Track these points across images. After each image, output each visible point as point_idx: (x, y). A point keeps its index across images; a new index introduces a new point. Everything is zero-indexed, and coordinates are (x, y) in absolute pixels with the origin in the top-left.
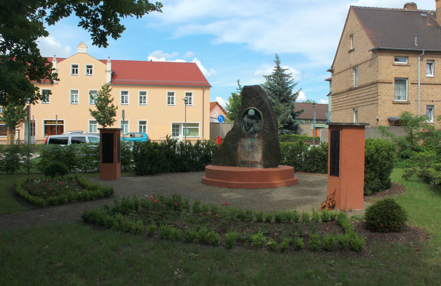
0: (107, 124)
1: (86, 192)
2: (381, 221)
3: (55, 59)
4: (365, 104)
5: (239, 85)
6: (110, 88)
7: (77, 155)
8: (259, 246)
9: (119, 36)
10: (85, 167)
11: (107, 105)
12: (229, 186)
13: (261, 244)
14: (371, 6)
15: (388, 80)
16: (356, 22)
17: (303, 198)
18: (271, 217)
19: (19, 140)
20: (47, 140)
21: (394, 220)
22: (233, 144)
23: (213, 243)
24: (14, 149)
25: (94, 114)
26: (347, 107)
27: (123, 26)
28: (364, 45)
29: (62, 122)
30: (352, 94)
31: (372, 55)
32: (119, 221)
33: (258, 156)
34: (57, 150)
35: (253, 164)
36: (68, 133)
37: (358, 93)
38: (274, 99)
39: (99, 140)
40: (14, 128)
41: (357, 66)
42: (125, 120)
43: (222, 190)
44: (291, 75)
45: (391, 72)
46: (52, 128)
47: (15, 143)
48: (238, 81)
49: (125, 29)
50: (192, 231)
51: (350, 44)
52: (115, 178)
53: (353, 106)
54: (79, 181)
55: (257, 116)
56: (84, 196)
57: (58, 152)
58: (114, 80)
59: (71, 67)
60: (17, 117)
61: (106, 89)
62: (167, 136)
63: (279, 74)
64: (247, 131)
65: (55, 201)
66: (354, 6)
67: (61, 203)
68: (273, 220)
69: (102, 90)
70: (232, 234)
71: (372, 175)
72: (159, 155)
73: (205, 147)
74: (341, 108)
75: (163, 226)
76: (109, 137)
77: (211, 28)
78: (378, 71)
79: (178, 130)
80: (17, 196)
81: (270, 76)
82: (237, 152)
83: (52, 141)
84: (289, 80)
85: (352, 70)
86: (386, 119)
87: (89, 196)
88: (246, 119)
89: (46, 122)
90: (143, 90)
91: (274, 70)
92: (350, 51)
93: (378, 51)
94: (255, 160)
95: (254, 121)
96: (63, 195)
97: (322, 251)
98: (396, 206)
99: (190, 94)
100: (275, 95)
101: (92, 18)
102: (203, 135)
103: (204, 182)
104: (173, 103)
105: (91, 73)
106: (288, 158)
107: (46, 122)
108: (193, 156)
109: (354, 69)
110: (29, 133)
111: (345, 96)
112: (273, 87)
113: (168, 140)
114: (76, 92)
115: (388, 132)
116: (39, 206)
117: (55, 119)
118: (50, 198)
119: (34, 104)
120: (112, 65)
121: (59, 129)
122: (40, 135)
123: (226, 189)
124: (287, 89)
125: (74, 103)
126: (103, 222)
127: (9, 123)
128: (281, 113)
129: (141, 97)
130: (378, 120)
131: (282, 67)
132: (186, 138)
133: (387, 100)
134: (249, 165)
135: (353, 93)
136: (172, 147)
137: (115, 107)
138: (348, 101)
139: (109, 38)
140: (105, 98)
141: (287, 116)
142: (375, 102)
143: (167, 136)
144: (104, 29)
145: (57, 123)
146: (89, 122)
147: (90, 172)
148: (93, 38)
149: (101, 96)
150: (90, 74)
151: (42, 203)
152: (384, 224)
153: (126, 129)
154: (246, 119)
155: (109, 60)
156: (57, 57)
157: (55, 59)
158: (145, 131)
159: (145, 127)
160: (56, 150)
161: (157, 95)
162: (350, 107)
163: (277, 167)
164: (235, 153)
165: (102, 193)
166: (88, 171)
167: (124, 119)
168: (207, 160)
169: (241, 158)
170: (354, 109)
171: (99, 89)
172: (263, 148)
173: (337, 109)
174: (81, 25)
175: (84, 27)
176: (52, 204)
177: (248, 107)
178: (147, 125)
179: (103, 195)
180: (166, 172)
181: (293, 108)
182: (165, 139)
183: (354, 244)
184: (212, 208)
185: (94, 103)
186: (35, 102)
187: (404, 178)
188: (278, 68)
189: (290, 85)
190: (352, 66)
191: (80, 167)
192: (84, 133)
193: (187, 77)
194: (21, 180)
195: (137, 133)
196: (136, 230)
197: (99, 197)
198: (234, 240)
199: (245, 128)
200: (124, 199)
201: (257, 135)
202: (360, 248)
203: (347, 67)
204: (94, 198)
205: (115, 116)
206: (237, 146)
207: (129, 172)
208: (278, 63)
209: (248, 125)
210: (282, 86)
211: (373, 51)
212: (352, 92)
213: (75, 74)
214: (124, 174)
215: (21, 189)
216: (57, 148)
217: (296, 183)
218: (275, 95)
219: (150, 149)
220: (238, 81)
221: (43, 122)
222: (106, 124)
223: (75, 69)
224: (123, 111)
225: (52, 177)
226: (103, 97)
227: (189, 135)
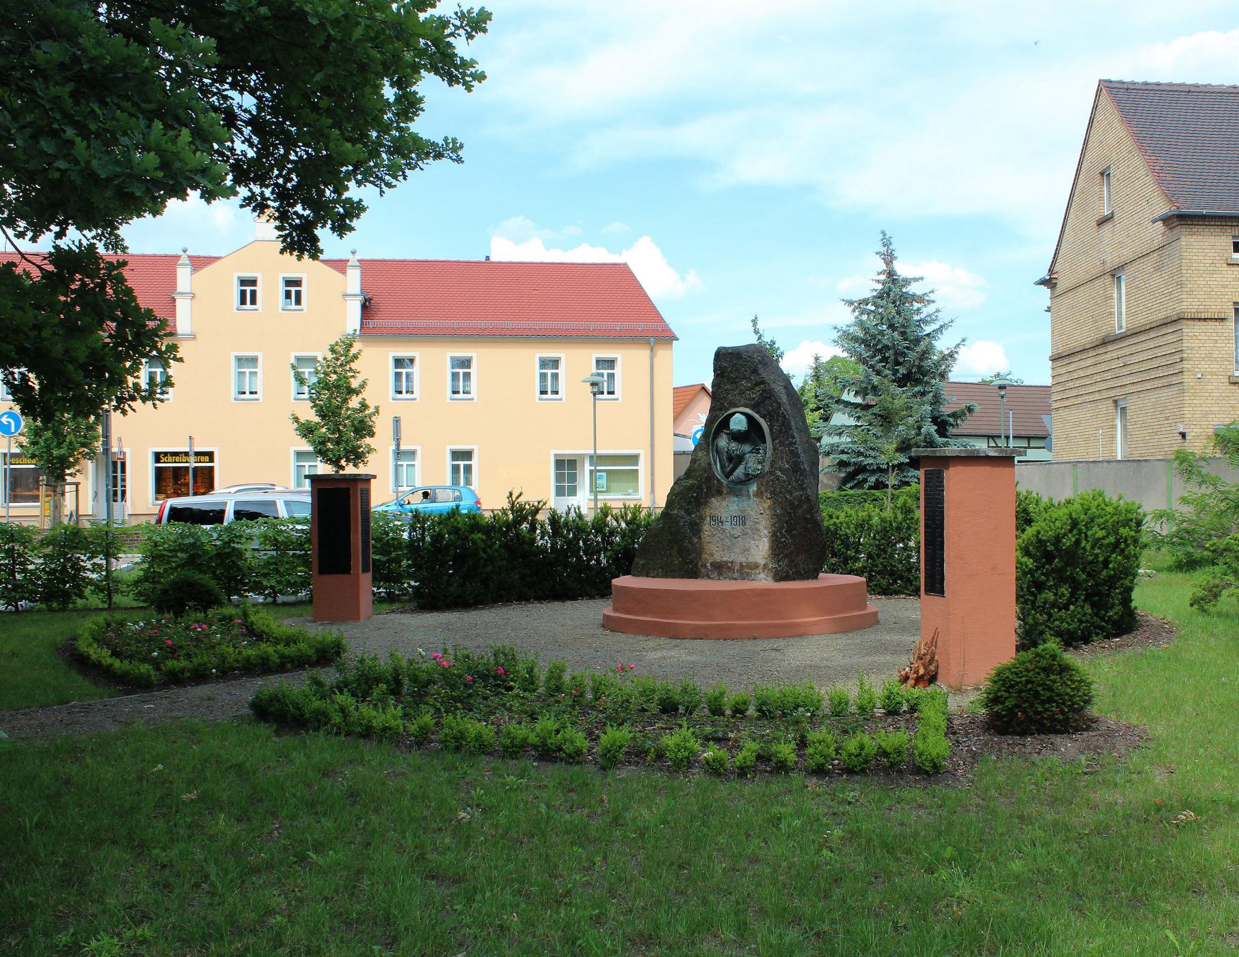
0: (348, 461)
1: (267, 648)
2: (1016, 706)
3: (184, 260)
4: (1148, 386)
5: (756, 332)
6: (353, 351)
7: (248, 555)
8: (685, 764)
9: (351, 229)
10: (272, 587)
11: (345, 401)
12: (674, 633)
13: (688, 758)
14: (1164, 80)
15: (1214, 309)
16: (1115, 131)
17: (838, 656)
18: (745, 703)
19: (76, 515)
20: (162, 511)
21: (1050, 700)
22: (690, 514)
23: (570, 756)
24: (71, 541)
25: (307, 430)
26: (1097, 396)
27: (361, 200)
28: (1142, 201)
29: (210, 455)
30: (1108, 356)
31: (1163, 235)
32: (343, 710)
33: (760, 549)
34: (192, 541)
35: (745, 571)
36: (226, 494)
37: (1127, 351)
38: (878, 373)
39: (306, 513)
40: (61, 477)
41: (1121, 267)
42: (402, 447)
43: (653, 642)
44: (932, 297)
45: (1223, 286)
46: (180, 475)
47: (66, 521)
48: (755, 322)
49: (364, 209)
50: (523, 732)
51: (1101, 198)
52: (356, 617)
53: (1112, 393)
54: (252, 623)
55: (753, 434)
56: (262, 658)
57: (193, 545)
58: (371, 324)
59: (236, 283)
60: (71, 443)
61: (343, 353)
62: (511, 494)
63: (892, 294)
64: (727, 475)
65: (183, 671)
66: (1110, 82)
67: (200, 676)
68: (752, 711)
69: (330, 356)
70: (615, 735)
71: (1063, 595)
72: (485, 552)
73: (623, 525)
74: (1080, 400)
75: (451, 717)
76: (337, 500)
77: (693, 136)
78: (1181, 285)
79: (573, 478)
80: (82, 663)
81: (866, 302)
82: (700, 538)
83: (177, 515)
84: (926, 311)
85: (1108, 279)
86: (1210, 432)
87: (275, 659)
88: (723, 442)
89: (158, 457)
90: (462, 352)
91: (878, 281)
92: (1102, 222)
93: (1179, 220)
94: (751, 559)
95: (747, 448)
96: (206, 659)
97: (841, 775)
98: (1060, 665)
99: (611, 363)
100: (881, 361)
101: (277, 185)
102: (653, 491)
103: (609, 624)
104: (557, 393)
105: (298, 302)
106: (870, 556)
107: (158, 457)
108: (591, 550)
109: (1113, 276)
110: (108, 491)
111: (1090, 362)
112: (873, 336)
113: (512, 509)
114: (253, 360)
115: (1204, 471)
116: (139, 685)
117: (187, 449)
118: (171, 664)
119: (124, 412)
120: (363, 275)
121: (199, 480)
122: (142, 500)
123: (663, 641)
124: (917, 341)
125: (248, 396)
126: (303, 715)
127: (49, 461)
128: (897, 419)
129: (455, 376)
130: (1183, 435)
131: (903, 269)
132: (596, 500)
133: (1212, 374)
134: (736, 575)
135: (1113, 351)
136: (525, 526)
137: (372, 410)
138: (1098, 378)
139: (324, 234)
140: (339, 380)
141: (919, 428)
142: (1175, 380)
143: (511, 494)
144: (308, 209)
145: (192, 459)
146: (292, 457)
147: (285, 604)
148: (281, 236)
149: (326, 374)
150: (294, 306)
151: (149, 676)
152: (1024, 712)
153: (411, 477)
154: (723, 442)
155: (353, 260)
156: (190, 253)
157: (184, 260)
158: (468, 482)
159: (468, 469)
160: (187, 541)
161: (505, 369)
162: (1105, 394)
163: (816, 578)
164: (696, 540)
165: (311, 652)
166: (280, 598)
167: (398, 445)
168: (625, 562)
169: (712, 555)
170: (1115, 402)
171: (322, 353)
172: (774, 525)
173: (1067, 403)
174: (248, 205)
175: (254, 210)
176: (175, 679)
177: (728, 409)
178: (474, 463)
179: (314, 658)
180: (508, 601)
181: (937, 401)
182: (506, 505)
183: (921, 755)
184: (594, 681)
185: (307, 396)
186: (126, 407)
187: (1195, 606)
188: (891, 274)
189: (928, 329)
190: (1108, 267)
191: (257, 588)
192: (277, 489)
193: (600, 309)
194: (87, 626)
195: (445, 488)
196: (385, 729)
197: (299, 663)
198: (620, 747)
199: (723, 467)
200: (362, 661)
201: (753, 488)
202: (935, 766)
203: (1095, 272)
204: (289, 666)
205: (372, 434)
206: (702, 519)
207: (399, 601)
208: (889, 258)
209: (730, 459)
210: (903, 333)
211: (1167, 220)
212: (1110, 348)
213: (248, 306)
214: (385, 606)
215: (90, 645)
216: (191, 535)
217: (873, 620)
218: (881, 361)
219: (457, 533)
220: (755, 322)
221: (150, 459)
222: (343, 463)
223: (248, 289)
224: (397, 421)
225: (177, 615)
226: (334, 377)
227: (608, 491)
